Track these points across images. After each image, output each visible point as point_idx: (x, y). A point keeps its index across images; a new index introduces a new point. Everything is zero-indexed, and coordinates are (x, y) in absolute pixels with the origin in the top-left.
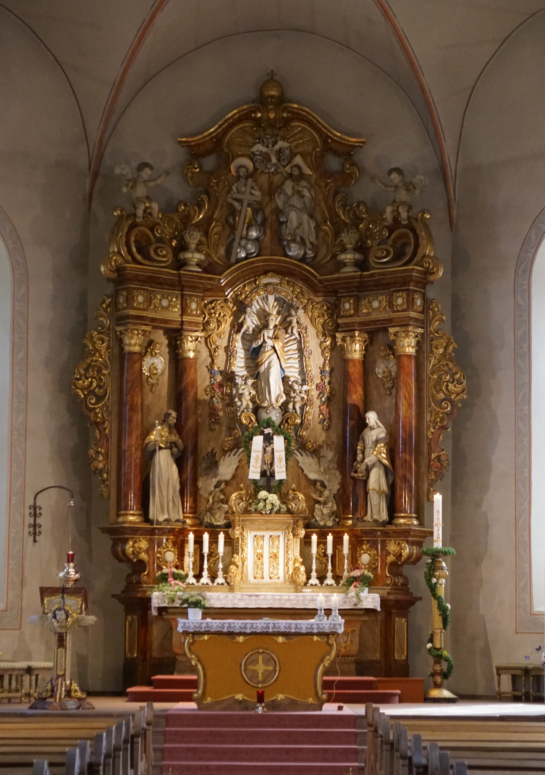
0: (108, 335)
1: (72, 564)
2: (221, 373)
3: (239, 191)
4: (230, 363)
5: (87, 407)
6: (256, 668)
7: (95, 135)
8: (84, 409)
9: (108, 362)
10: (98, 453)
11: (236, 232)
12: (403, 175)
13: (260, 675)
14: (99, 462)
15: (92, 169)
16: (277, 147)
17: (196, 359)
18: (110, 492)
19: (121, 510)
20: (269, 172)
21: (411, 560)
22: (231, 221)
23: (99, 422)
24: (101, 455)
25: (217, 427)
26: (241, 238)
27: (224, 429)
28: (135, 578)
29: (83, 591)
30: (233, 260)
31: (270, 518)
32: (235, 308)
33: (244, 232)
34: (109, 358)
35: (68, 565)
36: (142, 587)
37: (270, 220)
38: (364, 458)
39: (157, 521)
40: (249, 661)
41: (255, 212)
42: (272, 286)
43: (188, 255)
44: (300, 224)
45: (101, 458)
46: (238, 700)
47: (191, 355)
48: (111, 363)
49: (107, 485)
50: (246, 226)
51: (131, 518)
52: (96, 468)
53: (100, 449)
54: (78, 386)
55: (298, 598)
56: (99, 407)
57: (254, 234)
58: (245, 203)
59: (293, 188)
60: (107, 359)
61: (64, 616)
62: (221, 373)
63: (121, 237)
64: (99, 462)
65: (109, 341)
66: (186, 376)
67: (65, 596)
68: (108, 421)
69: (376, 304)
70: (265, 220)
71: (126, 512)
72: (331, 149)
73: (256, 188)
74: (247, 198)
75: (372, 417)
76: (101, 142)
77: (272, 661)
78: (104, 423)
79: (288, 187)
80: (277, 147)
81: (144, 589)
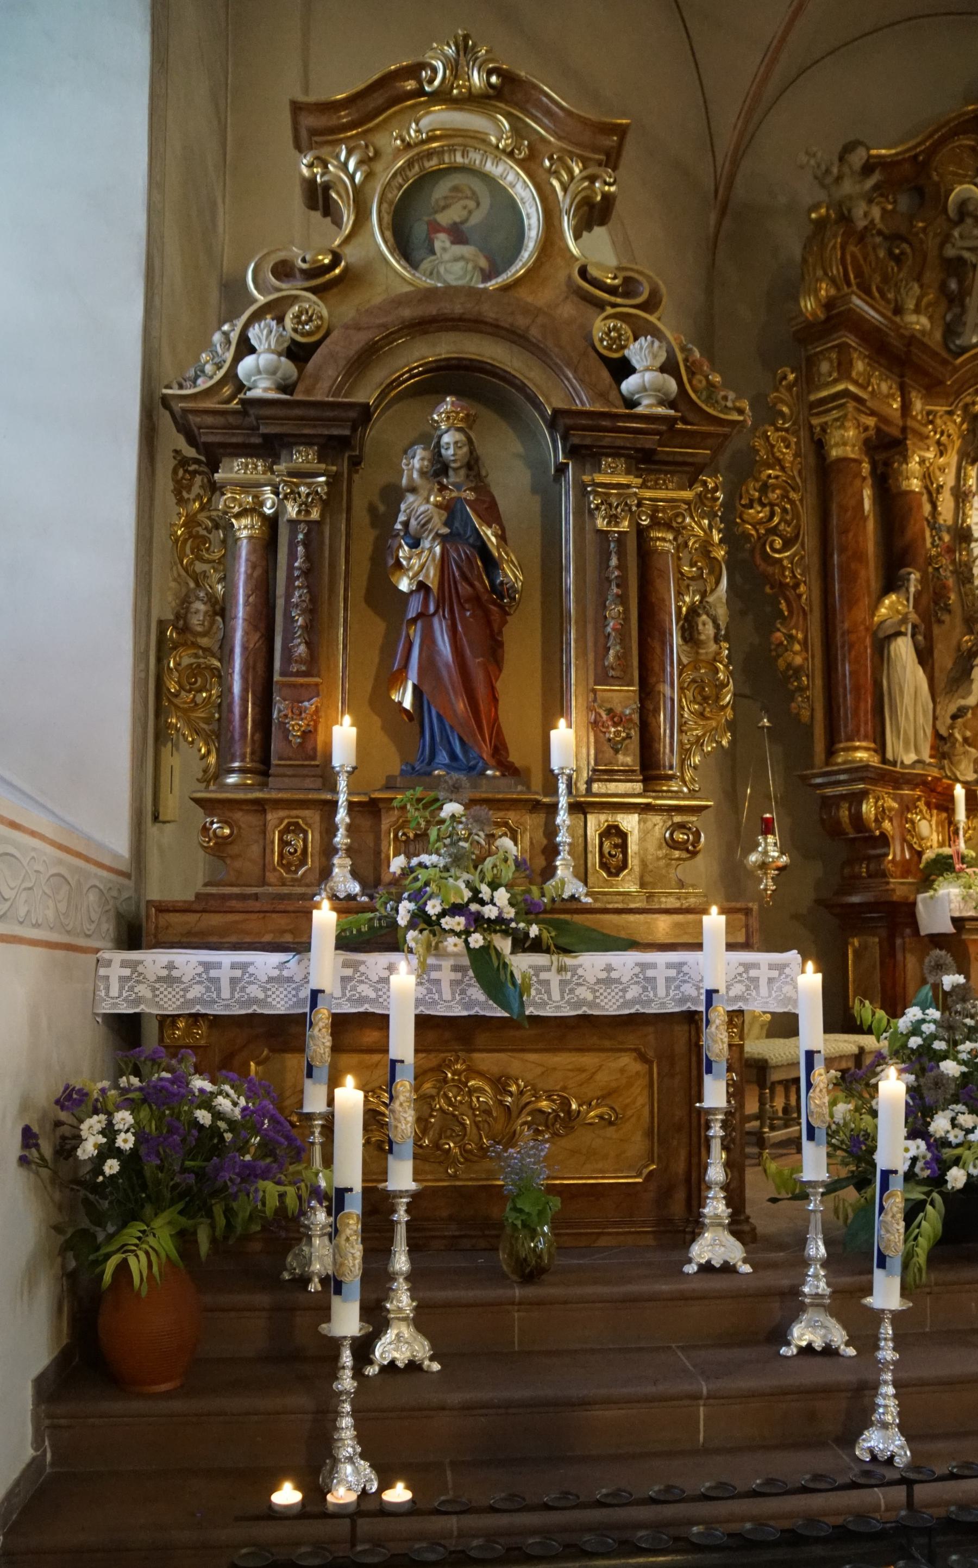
0: (796, 433)
1: (771, 839)
2: (949, 530)
4: (964, 514)
5: (766, 557)
7: (726, 140)
8: (759, 561)
9: (798, 480)
10: (791, 638)
11: (968, 300)
14: (795, 653)
15: (720, 197)
18: (813, 710)
19: (840, 742)
22: (953, 285)
23: (788, 584)
27: (958, 621)
28: (867, 868)
32: (965, 426)
34: (800, 472)
35: (765, 839)
36: (888, 883)
39: (902, 762)
42: (267, 874)
45: (797, 647)
47: (915, 484)
48: (804, 481)
49: (808, 698)
51: (860, 755)
52: (789, 666)
53: (794, 632)
54: (745, 517)
55: (753, 973)
56: (787, 557)
60: (796, 473)
62: (949, 530)
63: (834, 247)
64: (795, 653)
65: (797, 443)
66: (912, 522)
68: (805, 582)
71: (850, 744)
76: (736, 149)
78: (797, 585)
81: (892, 886)
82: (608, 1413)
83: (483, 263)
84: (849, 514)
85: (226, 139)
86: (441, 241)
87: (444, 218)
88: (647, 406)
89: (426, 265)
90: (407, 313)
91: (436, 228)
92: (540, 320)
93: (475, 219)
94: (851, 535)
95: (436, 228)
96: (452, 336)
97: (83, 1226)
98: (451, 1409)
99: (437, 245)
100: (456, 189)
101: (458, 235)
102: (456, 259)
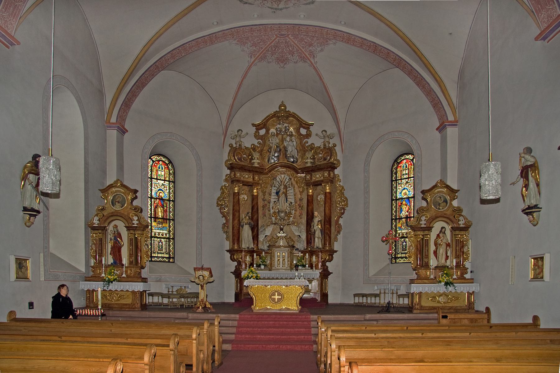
3: (272, 140)
6: (275, 297)
12: (65, 285)
13: (276, 300)
16: (284, 126)
17: (257, 195)
20: (282, 134)
21: (329, 260)
24: (226, 227)
25: (265, 218)
26: (273, 155)
29: (210, 269)
30: (270, 163)
31: (471, 248)
33: (274, 154)
37: (282, 150)
38: (314, 227)
40: (273, 294)
41: (277, 147)
43: (255, 161)
44: (292, 151)
46: (114, 238)
50: (274, 151)
57: (276, 155)
58: (274, 144)
59: (290, 139)
61: (202, 278)
67: (203, 271)
69: (318, 176)
70: (280, 150)
72: (302, 126)
73: (277, 139)
74: (274, 142)
75: (316, 213)
77: (280, 294)
79: (288, 139)
80: (284, 126)
82: (495, 347)
83: (121, 206)
84: (235, 203)
85: (556, 35)
86: (117, 203)
87: (117, 200)
88: (256, 165)
89: (115, 206)
90: (110, 215)
91: (116, 202)
92: (124, 215)
93: (121, 200)
94: (235, 207)
95: (116, 202)
96: (115, 217)
97: (317, 298)
98: (437, 249)
99: (116, 204)
100: (118, 197)
101: (118, 202)
102: (118, 205)
